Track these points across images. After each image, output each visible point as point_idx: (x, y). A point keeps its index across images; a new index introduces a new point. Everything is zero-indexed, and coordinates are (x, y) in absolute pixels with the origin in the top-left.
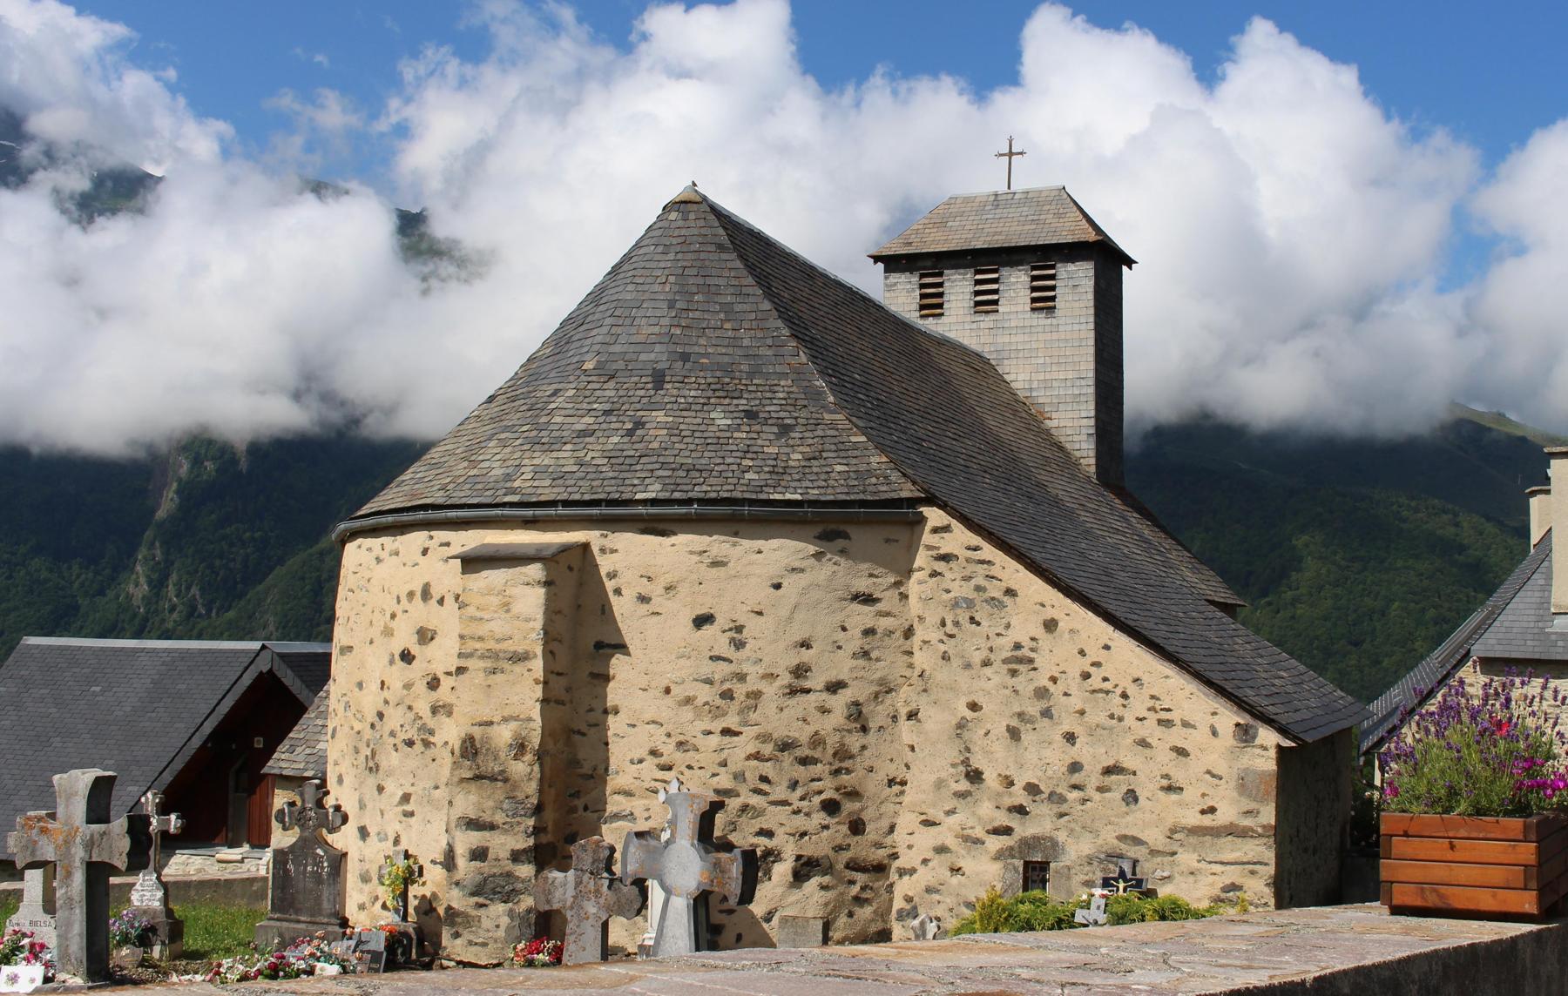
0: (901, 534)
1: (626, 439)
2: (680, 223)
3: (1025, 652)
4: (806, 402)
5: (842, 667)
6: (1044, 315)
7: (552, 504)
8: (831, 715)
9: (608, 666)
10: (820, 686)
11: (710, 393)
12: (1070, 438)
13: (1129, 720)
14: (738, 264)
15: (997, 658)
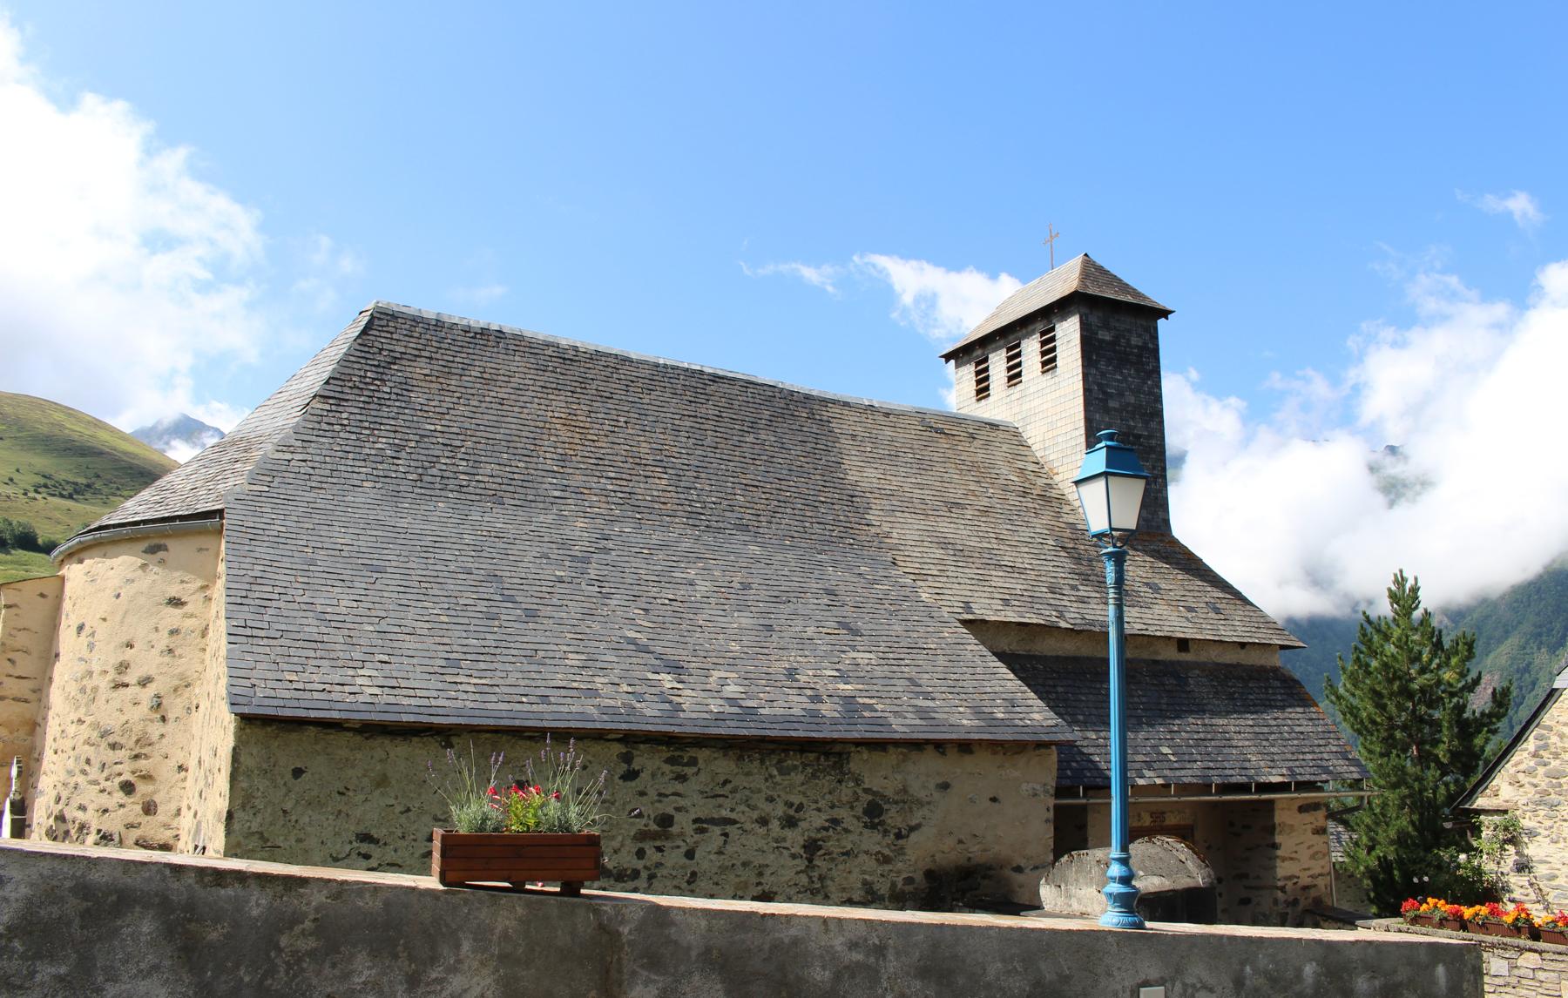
8: (140, 706)
10: (134, 681)
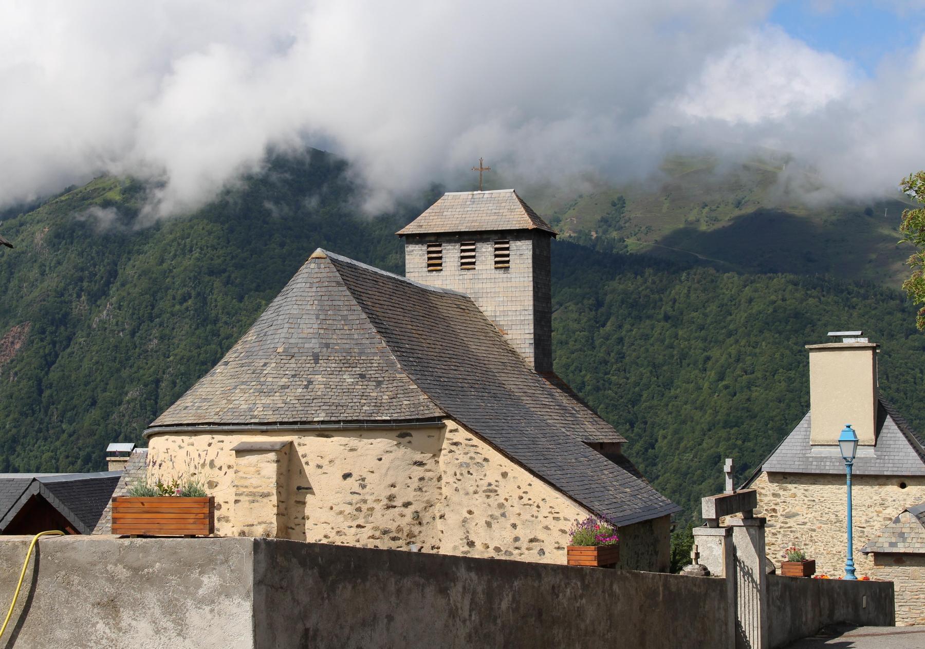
0: (434, 433)
1: (305, 390)
2: (317, 270)
3: (493, 487)
4: (387, 369)
5: (410, 495)
6: (503, 272)
7: (275, 423)
8: (406, 518)
9: (305, 498)
10: (400, 504)
11: (342, 365)
12: (519, 346)
13: (541, 518)
14: (348, 293)
15: (480, 490)
